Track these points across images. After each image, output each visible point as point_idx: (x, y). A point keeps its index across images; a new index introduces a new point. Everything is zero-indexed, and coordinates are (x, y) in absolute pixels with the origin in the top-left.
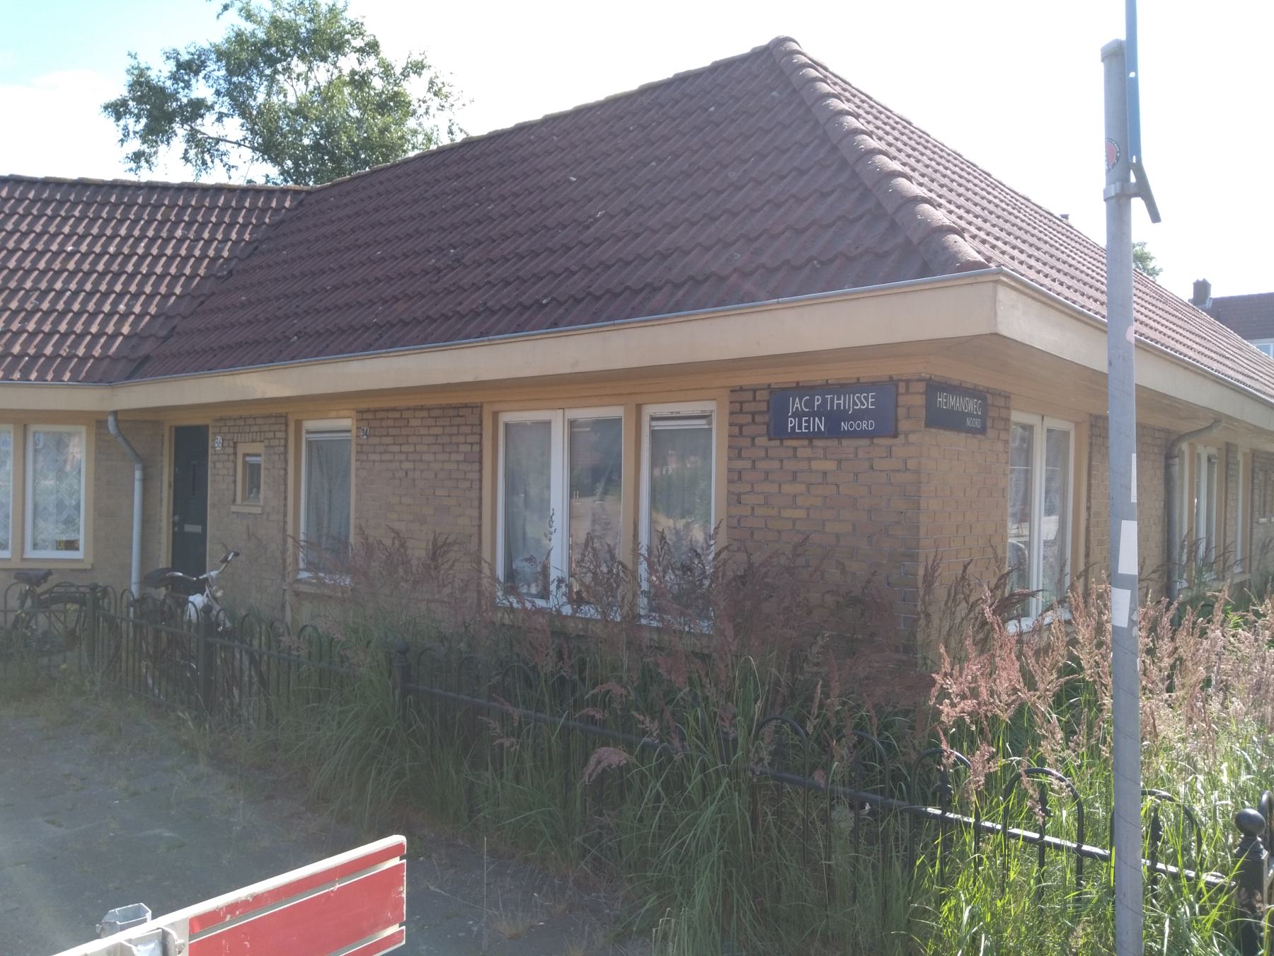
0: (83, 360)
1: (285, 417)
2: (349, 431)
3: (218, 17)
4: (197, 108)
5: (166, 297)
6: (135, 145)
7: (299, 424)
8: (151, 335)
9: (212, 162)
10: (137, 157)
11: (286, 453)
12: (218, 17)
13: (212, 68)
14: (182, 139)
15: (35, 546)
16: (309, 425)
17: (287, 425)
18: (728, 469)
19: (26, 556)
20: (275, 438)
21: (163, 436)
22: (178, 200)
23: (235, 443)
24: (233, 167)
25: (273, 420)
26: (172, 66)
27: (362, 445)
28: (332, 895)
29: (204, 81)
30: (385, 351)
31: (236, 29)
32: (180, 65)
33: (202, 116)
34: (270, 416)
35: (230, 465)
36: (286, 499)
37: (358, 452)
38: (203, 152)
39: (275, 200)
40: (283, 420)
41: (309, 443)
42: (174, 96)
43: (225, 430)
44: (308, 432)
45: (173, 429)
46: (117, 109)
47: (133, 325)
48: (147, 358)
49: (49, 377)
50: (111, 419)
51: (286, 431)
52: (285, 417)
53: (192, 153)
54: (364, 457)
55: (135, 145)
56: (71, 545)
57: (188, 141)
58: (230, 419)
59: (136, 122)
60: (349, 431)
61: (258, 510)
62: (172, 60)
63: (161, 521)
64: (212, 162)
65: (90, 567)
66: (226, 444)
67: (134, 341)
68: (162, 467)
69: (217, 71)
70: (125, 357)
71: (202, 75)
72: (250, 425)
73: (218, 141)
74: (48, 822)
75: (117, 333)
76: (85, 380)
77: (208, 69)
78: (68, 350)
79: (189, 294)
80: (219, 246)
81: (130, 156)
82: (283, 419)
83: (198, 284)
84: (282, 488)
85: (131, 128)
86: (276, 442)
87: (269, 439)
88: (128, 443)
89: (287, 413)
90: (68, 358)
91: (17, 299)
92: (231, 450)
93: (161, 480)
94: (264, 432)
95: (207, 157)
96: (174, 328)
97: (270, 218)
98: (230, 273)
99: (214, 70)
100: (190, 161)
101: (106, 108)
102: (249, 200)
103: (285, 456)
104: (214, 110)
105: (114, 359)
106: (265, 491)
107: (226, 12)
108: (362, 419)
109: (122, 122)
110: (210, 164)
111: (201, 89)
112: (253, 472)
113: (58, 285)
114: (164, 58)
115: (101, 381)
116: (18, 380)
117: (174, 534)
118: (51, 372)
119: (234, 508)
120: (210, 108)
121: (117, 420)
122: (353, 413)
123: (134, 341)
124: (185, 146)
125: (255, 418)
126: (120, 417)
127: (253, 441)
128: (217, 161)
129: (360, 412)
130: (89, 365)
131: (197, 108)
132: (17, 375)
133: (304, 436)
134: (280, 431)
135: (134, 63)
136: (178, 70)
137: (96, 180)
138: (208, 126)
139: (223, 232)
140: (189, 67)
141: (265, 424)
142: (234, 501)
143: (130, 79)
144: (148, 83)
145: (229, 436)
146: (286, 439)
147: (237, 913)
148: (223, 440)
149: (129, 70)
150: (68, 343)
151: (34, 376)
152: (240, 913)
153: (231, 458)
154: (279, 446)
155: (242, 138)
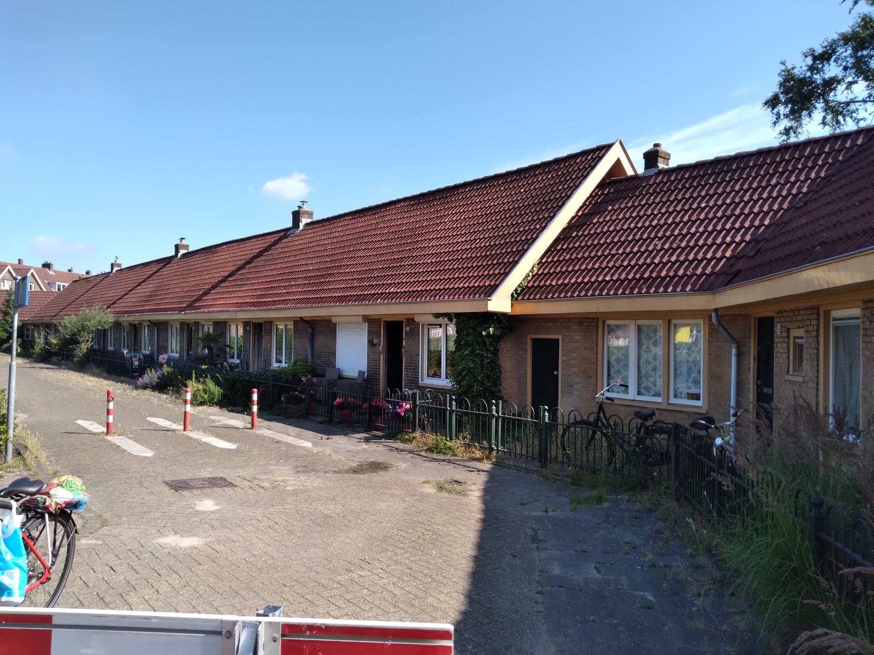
0: (700, 276)
1: (817, 308)
2: (859, 318)
3: (850, 12)
4: (830, 84)
5: (758, 228)
6: (785, 123)
7: (827, 313)
8: (745, 255)
9: (844, 120)
10: (787, 132)
11: (818, 336)
12: (850, 12)
13: (840, 52)
14: (820, 110)
15: (675, 396)
16: (835, 314)
17: (818, 315)
18: (261, 324)
19: (670, 402)
20: (811, 325)
21: (750, 325)
22: (776, 158)
23: (788, 329)
24: (861, 119)
25: (809, 312)
26: (809, 61)
27: (866, 329)
28: (386, 647)
29: (835, 63)
30: (864, 249)
31: (862, 16)
32: (815, 58)
33: (835, 89)
34: (807, 308)
35: (785, 345)
36: (818, 371)
37: (864, 335)
38: (837, 115)
39: (850, 141)
40: (815, 311)
41: (836, 329)
42: (812, 82)
43: (782, 319)
44: (835, 320)
45: (757, 320)
46: (773, 102)
47: (734, 250)
48: (739, 272)
49: (678, 290)
50: (714, 314)
51: (818, 319)
52: (817, 308)
53: (829, 117)
54: (868, 339)
55: (785, 123)
56: (696, 397)
57: (826, 110)
58: (785, 311)
59: (785, 107)
60: (859, 318)
61: (801, 379)
62: (809, 57)
63: (749, 384)
64: (844, 120)
65: (705, 412)
66: (783, 330)
67: (732, 261)
68: (750, 347)
69: (845, 52)
70: (725, 272)
71: (833, 59)
72: (796, 316)
73: (848, 104)
74: (596, 568)
75: (723, 257)
76: (699, 290)
77: (837, 54)
78: (692, 271)
79: (774, 223)
80: (801, 185)
81: (782, 132)
82: (816, 310)
83: (782, 215)
84: (815, 363)
85: (782, 113)
86: (811, 328)
87: (807, 326)
88: (726, 330)
89: (818, 305)
90: (691, 277)
91: (669, 242)
92: (785, 334)
93: (750, 355)
94: (805, 320)
95: (840, 118)
96: (760, 248)
97: (843, 156)
98: (806, 204)
99: (843, 53)
100: (828, 124)
101: (766, 104)
102: (828, 146)
103: (817, 339)
104: (844, 81)
105: (718, 275)
106: (806, 366)
107: (857, 6)
108: (867, 308)
109: (775, 111)
110: (842, 122)
111: (832, 70)
112: (799, 348)
113: (693, 230)
114: (804, 58)
115: (708, 289)
116: (662, 292)
117: (758, 392)
118: (680, 286)
119: (787, 377)
120: (839, 82)
121: (717, 315)
122: (860, 304)
123: (732, 261)
124: (823, 114)
125: (799, 310)
126: (719, 313)
127: (799, 328)
128: (848, 119)
129: (865, 302)
130: (702, 279)
131: (830, 84)
132: (662, 289)
133: (832, 323)
134: (814, 319)
135: (783, 68)
136: (814, 62)
137: (725, 157)
138: (840, 94)
139: (805, 175)
140: (825, 57)
141: (805, 314)
142: (788, 371)
143: (781, 79)
144: (793, 79)
145: (784, 324)
146: (818, 326)
147: (314, 632)
148: (781, 327)
149: (780, 74)
150: (692, 267)
151: (670, 289)
152: (316, 633)
153: (786, 340)
154: (813, 331)
155: (867, 96)
